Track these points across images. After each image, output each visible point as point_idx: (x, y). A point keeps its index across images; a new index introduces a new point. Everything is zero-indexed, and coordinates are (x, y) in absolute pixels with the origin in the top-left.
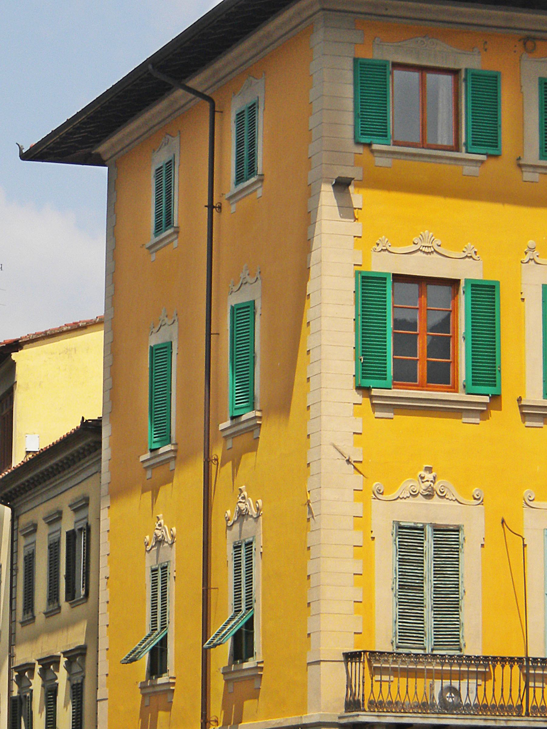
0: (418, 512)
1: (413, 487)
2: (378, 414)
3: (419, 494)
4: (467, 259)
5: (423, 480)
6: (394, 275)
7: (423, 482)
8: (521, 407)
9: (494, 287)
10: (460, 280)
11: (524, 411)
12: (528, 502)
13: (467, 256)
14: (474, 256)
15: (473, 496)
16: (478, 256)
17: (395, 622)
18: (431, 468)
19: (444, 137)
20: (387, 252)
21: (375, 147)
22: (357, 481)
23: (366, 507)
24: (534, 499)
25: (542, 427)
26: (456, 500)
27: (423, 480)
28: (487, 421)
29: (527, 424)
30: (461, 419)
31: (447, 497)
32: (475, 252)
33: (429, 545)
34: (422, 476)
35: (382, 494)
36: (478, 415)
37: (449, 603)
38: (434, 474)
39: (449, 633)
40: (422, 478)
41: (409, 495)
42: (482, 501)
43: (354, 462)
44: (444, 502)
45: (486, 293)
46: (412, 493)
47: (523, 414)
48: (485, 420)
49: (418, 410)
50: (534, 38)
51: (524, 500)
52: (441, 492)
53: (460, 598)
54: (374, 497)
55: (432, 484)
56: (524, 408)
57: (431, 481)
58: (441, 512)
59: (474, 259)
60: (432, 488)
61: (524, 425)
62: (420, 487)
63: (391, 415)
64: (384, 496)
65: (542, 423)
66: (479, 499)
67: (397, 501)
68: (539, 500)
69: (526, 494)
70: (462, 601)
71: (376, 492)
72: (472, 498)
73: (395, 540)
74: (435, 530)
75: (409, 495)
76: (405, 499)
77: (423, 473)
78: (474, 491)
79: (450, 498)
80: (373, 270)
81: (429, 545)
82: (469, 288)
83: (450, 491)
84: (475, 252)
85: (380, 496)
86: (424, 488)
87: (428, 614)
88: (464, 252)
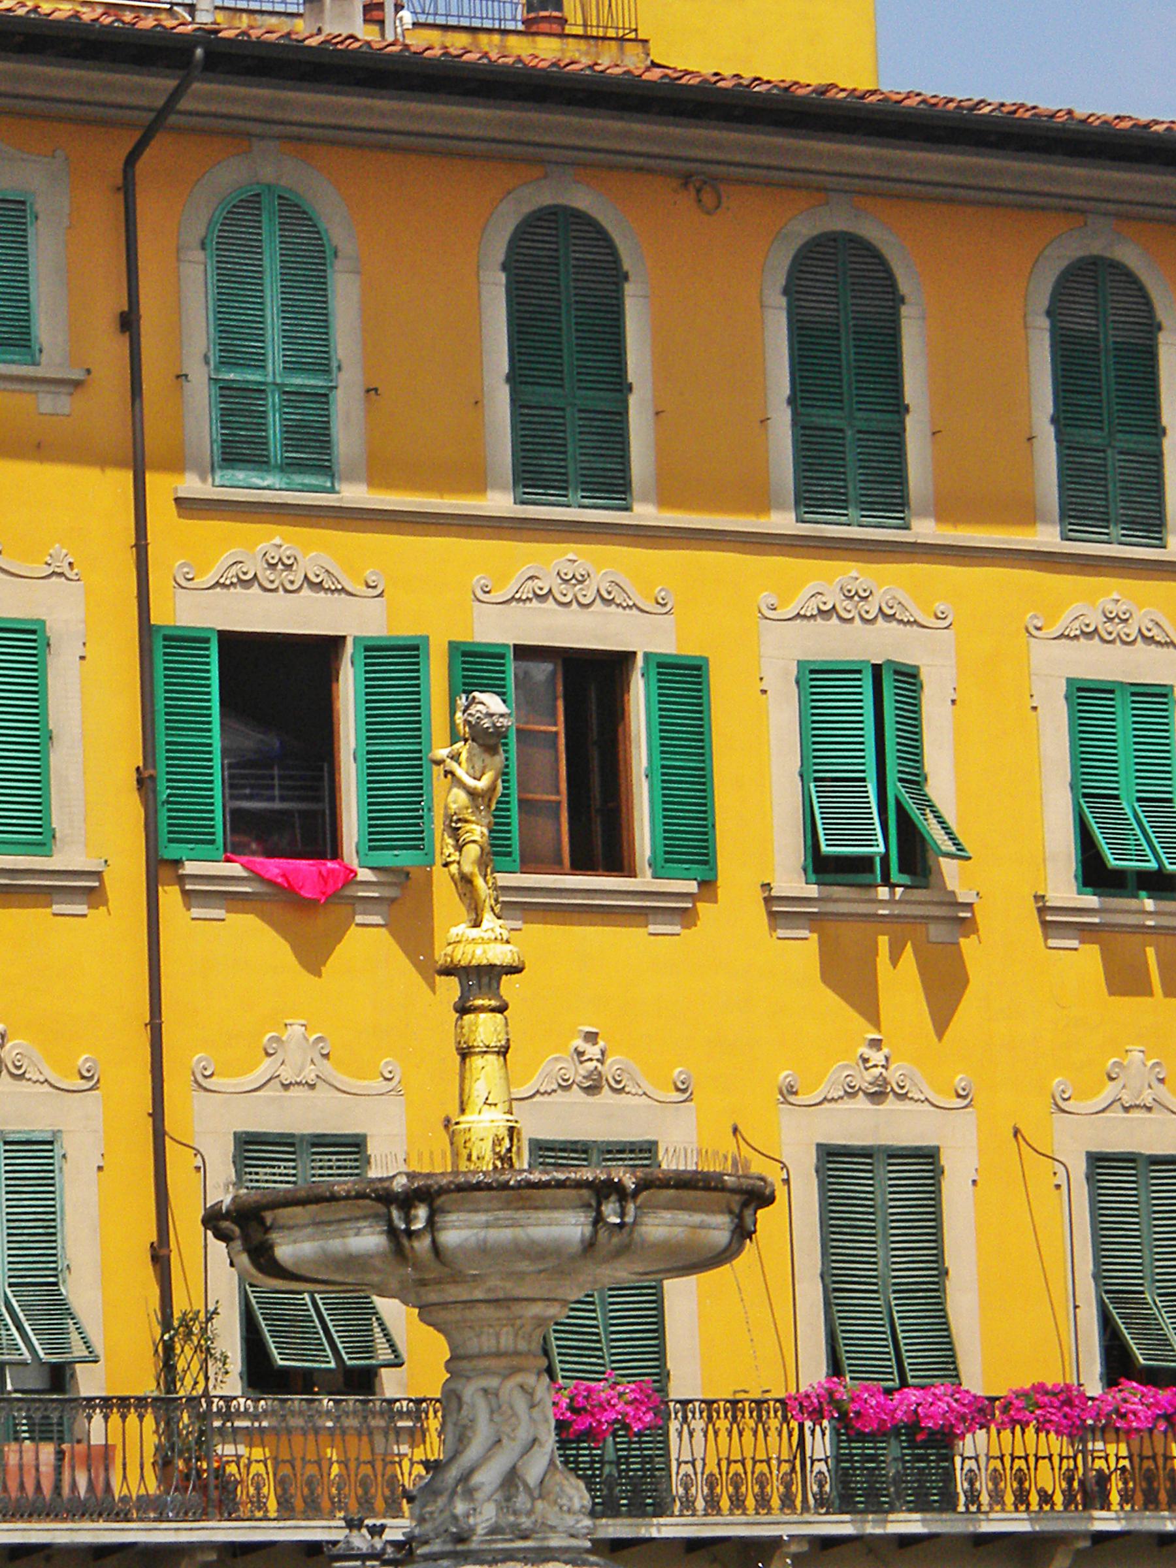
0: (858, 1125)
1: (563, 1071)
2: (196, 912)
3: (575, 1086)
4: (54, 579)
5: (868, 1065)
6: (516, 647)
7: (867, 1069)
8: (768, 900)
9: (699, 668)
10: (635, 653)
11: (775, 909)
12: (200, 1079)
13: (54, 573)
15: (956, 1092)
16: (76, 571)
20: (63, 579)
24: (212, 1075)
25: (84, 916)
27: (868, 1065)
28: (694, 929)
29: (781, 933)
30: (49, 905)
32: (70, 564)
34: (581, 1049)
35: (796, 1093)
36: (677, 918)
38: (885, 1050)
40: (866, 1060)
41: (555, 1086)
42: (98, 1081)
44: (908, 1106)
45: (684, 679)
46: (849, 1090)
47: (772, 915)
48: (689, 928)
49: (572, 912)
51: (193, 1074)
52: (614, 1078)
54: (782, 1100)
55: (599, 1065)
56: (775, 902)
57: (598, 1060)
59: (68, 579)
60: (885, 1079)
63: (220, 913)
64: (799, 1097)
65: (223, 911)
66: (965, 1097)
67: (823, 1106)
68: (222, 1075)
69: (200, 1061)
71: (785, 1092)
72: (673, 1087)
75: (555, 1086)
76: (549, 1094)
77: (579, 1043)
78: (959, 1080)
79: (34, 1078)
80: (478, 639)
82: (653, 671)
83: (632, 1079)
84: (70, 564)
85: (792, 1099)
86: (869, 1079)
88: (47, 563)
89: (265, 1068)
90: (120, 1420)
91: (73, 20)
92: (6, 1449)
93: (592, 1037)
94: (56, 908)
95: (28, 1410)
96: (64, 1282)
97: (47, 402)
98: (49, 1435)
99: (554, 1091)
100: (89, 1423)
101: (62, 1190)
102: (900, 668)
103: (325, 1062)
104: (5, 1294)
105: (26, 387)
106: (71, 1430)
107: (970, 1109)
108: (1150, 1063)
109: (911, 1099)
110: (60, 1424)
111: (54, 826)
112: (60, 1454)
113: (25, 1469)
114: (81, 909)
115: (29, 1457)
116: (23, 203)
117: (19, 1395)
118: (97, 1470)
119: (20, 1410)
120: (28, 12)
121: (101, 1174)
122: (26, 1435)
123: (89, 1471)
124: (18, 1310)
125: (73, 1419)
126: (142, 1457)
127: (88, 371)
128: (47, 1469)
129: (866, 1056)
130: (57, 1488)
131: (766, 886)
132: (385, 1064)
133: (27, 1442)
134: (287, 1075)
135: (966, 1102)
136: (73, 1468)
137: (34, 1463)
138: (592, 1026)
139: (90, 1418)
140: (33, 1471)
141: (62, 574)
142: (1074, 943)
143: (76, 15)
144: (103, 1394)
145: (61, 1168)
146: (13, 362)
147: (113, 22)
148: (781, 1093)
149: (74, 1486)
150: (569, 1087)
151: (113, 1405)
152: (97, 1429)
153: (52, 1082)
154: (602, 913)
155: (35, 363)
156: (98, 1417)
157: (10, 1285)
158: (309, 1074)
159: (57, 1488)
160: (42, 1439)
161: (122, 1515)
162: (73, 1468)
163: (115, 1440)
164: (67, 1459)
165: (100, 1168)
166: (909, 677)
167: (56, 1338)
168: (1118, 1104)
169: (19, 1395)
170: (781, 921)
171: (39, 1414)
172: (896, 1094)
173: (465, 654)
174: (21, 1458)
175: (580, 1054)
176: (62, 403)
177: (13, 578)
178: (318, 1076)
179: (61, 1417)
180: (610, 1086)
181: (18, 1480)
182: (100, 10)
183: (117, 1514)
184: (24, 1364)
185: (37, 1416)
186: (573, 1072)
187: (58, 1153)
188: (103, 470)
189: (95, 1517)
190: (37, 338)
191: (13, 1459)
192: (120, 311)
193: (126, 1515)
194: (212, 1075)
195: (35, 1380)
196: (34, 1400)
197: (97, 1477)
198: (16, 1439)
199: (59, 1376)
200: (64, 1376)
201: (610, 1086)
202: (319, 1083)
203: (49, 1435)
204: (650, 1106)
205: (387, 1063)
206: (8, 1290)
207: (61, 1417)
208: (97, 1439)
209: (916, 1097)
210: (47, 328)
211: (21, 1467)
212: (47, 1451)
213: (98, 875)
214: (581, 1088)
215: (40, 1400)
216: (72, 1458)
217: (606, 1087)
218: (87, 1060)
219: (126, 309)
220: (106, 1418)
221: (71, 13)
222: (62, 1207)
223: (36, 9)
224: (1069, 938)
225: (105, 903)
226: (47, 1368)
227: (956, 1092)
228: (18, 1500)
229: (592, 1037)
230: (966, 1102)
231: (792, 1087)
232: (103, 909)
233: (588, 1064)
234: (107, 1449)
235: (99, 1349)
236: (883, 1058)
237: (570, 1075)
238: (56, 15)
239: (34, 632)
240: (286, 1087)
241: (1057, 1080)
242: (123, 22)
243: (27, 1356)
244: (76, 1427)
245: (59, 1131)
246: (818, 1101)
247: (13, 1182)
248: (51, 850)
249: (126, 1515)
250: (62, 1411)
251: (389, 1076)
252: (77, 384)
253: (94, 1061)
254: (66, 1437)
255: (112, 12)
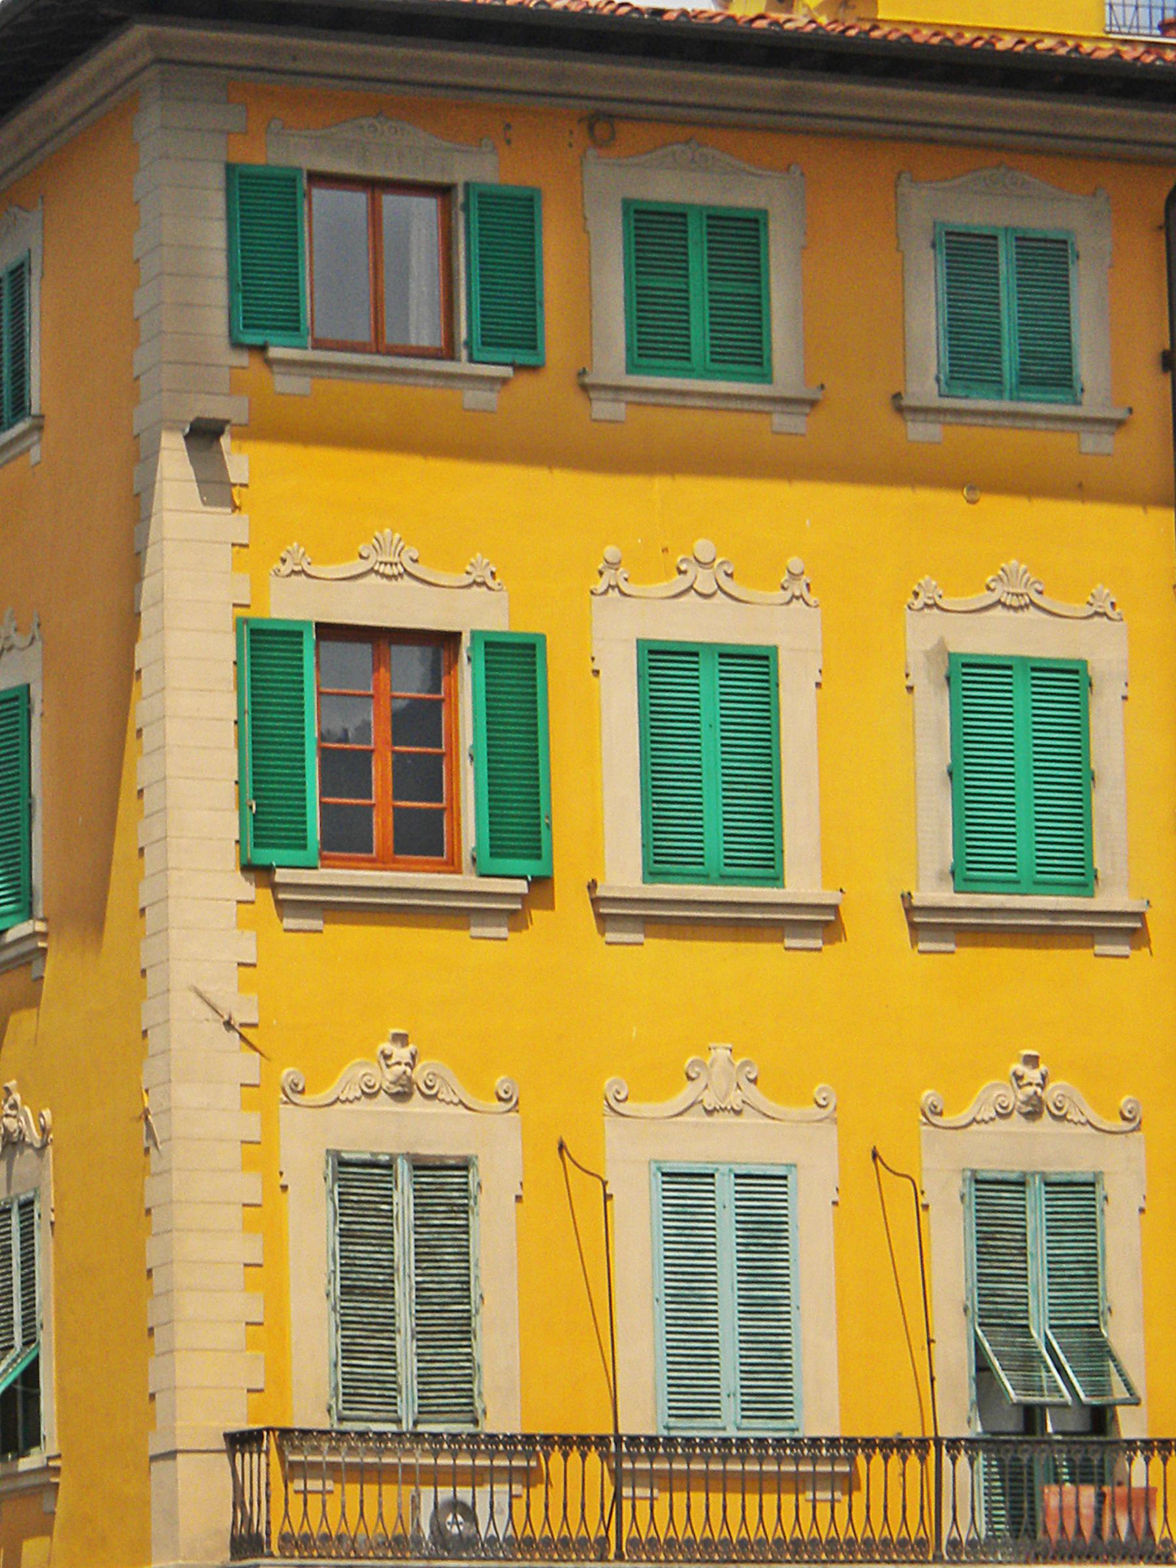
1: (1000, 1099)
5: (389, 1063)
7: (1020, 1087)
10: (460, 634)
12: (613, 1103)
13: (475, 583)
14: (490, 582)
15: (1121, 1114)
16: (498, 580)
17: (336, 1365)
18: (1037, 1057)
19: (423, 329)
21: (274, 353)
22: (247, 1065)
23: (269, 1120)
24: (626, 1099)
25: (1127, 957)
26: (461, 1102)
31: (440, 1096)
32: (493, 574)
33: (403, 1199)
35: (941, 1114)
36: (819, 931)
37: (450, 1322)
39: (452, 1380)
42: (1140, 1122)
43: (241, 1025)
45: (516, 662)
46: (366, 1090)
50: (610, 117)
52: (1055, 1105)
53: (473, 1311)
56: (602, 903)
58: (431, 1129)
59: (489, 588)
61: (604, 940)
62: (383, 1076)
69: (610, 1086)
70: (478, 1318)
73: (332, 1192)
74: (416, 1168)
78: (499, 1082)
79: (448, 1100)
81: (403, 1199)
84: (493, 574)
85: (935, 1120)
86: (391, 1077)
87: (406, 1347)
88: (468, 573)
89: (687, 1093)
90: (882, 1462)
91: (1114, 59)
92: (1046, 1491)
93: (1032, 1061)
94: (1098, 949)
95: (1069, 1452)
96: (1105, 1324)
97: (1091, 442)
98: (1090, 1477)
99: (358, 1099)
100: (1130, 1464)
101: (1103, 1232)
102: (655, 647)
103: (752, 1086)
104: (1046, 1336)
105: (1068, 426)
106: (1112, 1473)
107: (512, 1114)
108: (737, 1063)
109: (442, 1100)
110: (1101, 1467)
111: (1096, 866)
112: (1101, 1497)
113: (1065, 1511)
114: (1124, 950)
115: (1069, 1500)
116: (1065, 242)
117: (1059, 1437)
118: (1138, 1514)
119: (1060, 1452)
120: (1069, 52)
121: (1143, 1216)
122: (1067, 1477)
123: (1130, 1513)
124: (1059, 1351)
125: (1114, 1461)
126: (904, 1499)
127: (1130, 410)
128: (1087, 1511)
129: (1020, 1073)
130: (1098, 1530)
131: (906, 897)
132: (818, 1090)
133: (1068, 1485)
134: (710, 1101)
135: (1133, 1125)
136: (1113, 1512)
137: (1074, 1506)
138: (1033, 1048)
139: (1130, 1460)
140: (1073, 1514)
141: (1105, 614)
142: (639, 937)
143: (1118, 54)
144: (1145, 1436)
145: (1102, 1211)
146: (1056, 402)
147: (1153, 61)
148: (924, 1114)
149: (1115, 1529)
150: (375, 1094)
151: (1138, 1448)
152: (1138, 1472)
153: (1095, 1124)
154: (360, 912)
155: (1078, 403)
156: (1139, 1459)
157: (1051, 1327)
158: (735, 1100)
159: (1098, 1530)
160: (1083, 1481)
161: (1163, 1558)
162: (1113, 1512)
163: (1156, 1482)
164: (1107, 1502)
165: (1142, 1210)
166: (754, 665)
167: (1098, 1383)
168: (698, 1107)
169: (1059, 1437)
170: (609, 924)
171: (1079, 1456)
172: (1053, 1116)
173: (488, 645)
174: (1061, 1500)
175: (1018, 1078)
176: (1104, 442)
177: (1052, 618)
178: (744, 1102)
179: (1102, 1460)
180: (1050, 1112)
181: (1058, 1522)
182: (1141, 49)
183: (1159, 1557)
184: (1065, 1406)
185: (1078, 1458)
186: (379, 1078)
187: (1099, 1195)
188: (1145, 511)
189: (1136, 1559)
190: (1079, 377)
191: (1053, 1502)
192: (1161, 350)
193: (1167, 1558)
194: (626, 1099)
195: (1075, 1422)
196: (1074, 1442)
197: (1138, 1520)
198: (1057, 1481)
199: (1100, 1419)
200: (1104, 1418)
201: (1050, 1112)
202: (746, 1108)
203: (1090, 1477)
204: (1093, 1136)
205: (820, 1090)
206: (1049, 1333)
207: (1102, 1460)
208: (1138, 1481)
209: (1076, 1119)
210: (1089, 366)
211: (1061, 1509)
212: (1088, 1494)
213: (1139, 916)
214: (1020, 1113)
215: (1080, 1443)
216: (1113, 1499)
217: (1046, 1112)
218: (1130, 1101)
219: (1168, 347)
220: (1147, 1460)
221: (1112, 52)
222: (1104, 1251)
223: (1077, 48)
224: (633, 932)
225: (1148, 943)
226: (1088, 1410)
227: (1121, 1114)
228: (1058, 1542)
229: (1032, 1061)
230: (1133, 1125)
231: (935, 1107)
232: (1146, 950)
233: (397, 1067)
234: (1148, 1492)
235: (1141, 1392)
236: (1039, 1076)
237: (1010, 1101)
238: (1097, 55)
239: (1076, 672)
240: (709, 1113)
241: (608, 1081)
242: (1164, 60)
243: (1068, 1397)
244: (1117, 1469)
245: (1101, 1173)
246: (963, 1123)
247: (1054, 1224)
248: (1093, 890)
249: (1167, 1558)
250: (1103, 1453)
251: (823, 1103)
252: (1119, 423)
253: (1136, 1102)
254: (1107, 1476)
255: (1153, 50)
